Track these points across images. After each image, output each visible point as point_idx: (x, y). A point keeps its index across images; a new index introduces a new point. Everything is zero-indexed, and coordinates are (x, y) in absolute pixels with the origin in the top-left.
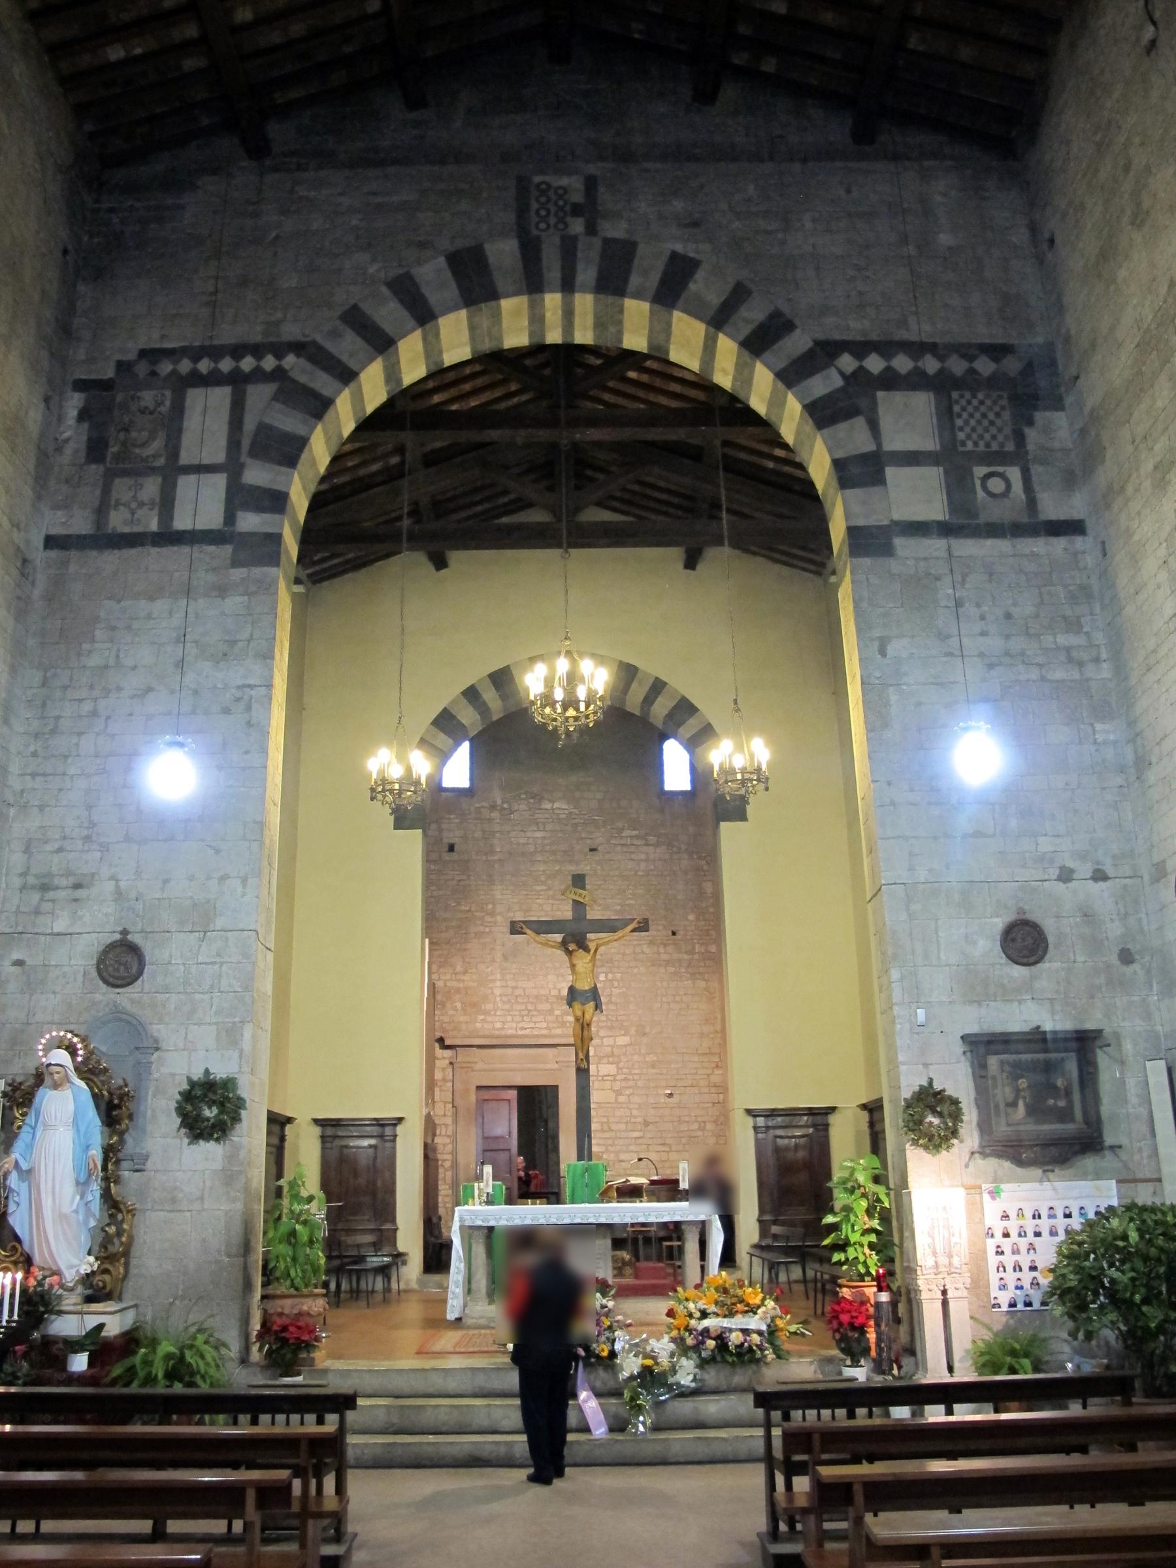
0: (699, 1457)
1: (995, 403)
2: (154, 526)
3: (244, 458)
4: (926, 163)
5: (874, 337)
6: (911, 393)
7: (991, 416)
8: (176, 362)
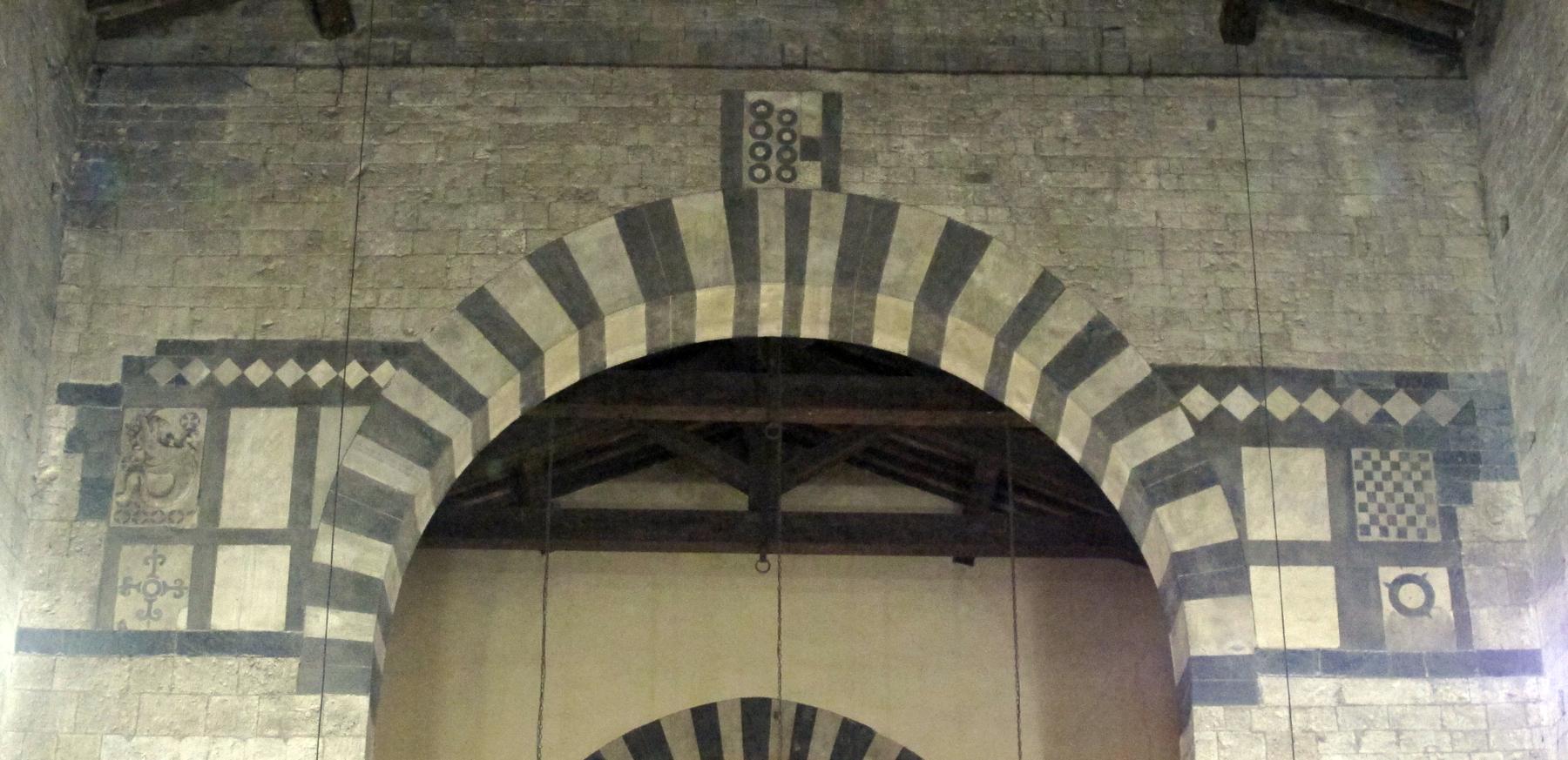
0: (338, 433)
1: (1415, 467)
2: (182, 623)
3: (317, 522)
4: (1329, 82)
5: (1240, 361)
6: (1291, 450)
7: (1409, 487)
8: (213, 365)
